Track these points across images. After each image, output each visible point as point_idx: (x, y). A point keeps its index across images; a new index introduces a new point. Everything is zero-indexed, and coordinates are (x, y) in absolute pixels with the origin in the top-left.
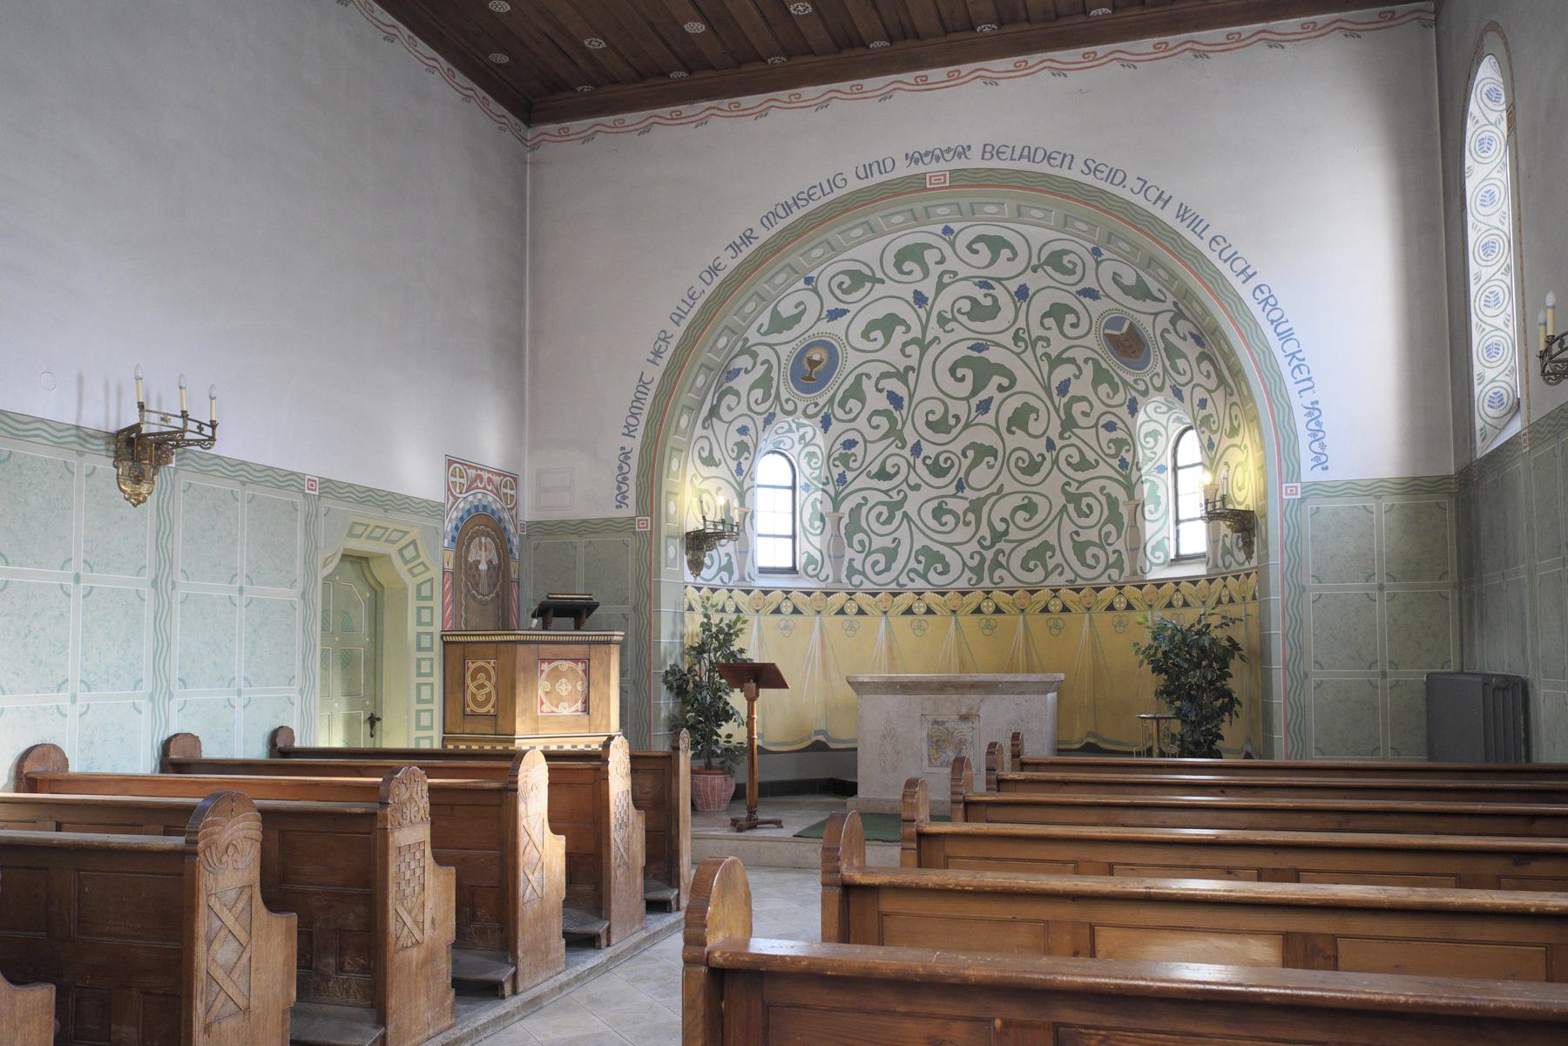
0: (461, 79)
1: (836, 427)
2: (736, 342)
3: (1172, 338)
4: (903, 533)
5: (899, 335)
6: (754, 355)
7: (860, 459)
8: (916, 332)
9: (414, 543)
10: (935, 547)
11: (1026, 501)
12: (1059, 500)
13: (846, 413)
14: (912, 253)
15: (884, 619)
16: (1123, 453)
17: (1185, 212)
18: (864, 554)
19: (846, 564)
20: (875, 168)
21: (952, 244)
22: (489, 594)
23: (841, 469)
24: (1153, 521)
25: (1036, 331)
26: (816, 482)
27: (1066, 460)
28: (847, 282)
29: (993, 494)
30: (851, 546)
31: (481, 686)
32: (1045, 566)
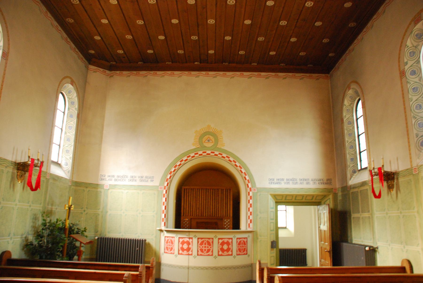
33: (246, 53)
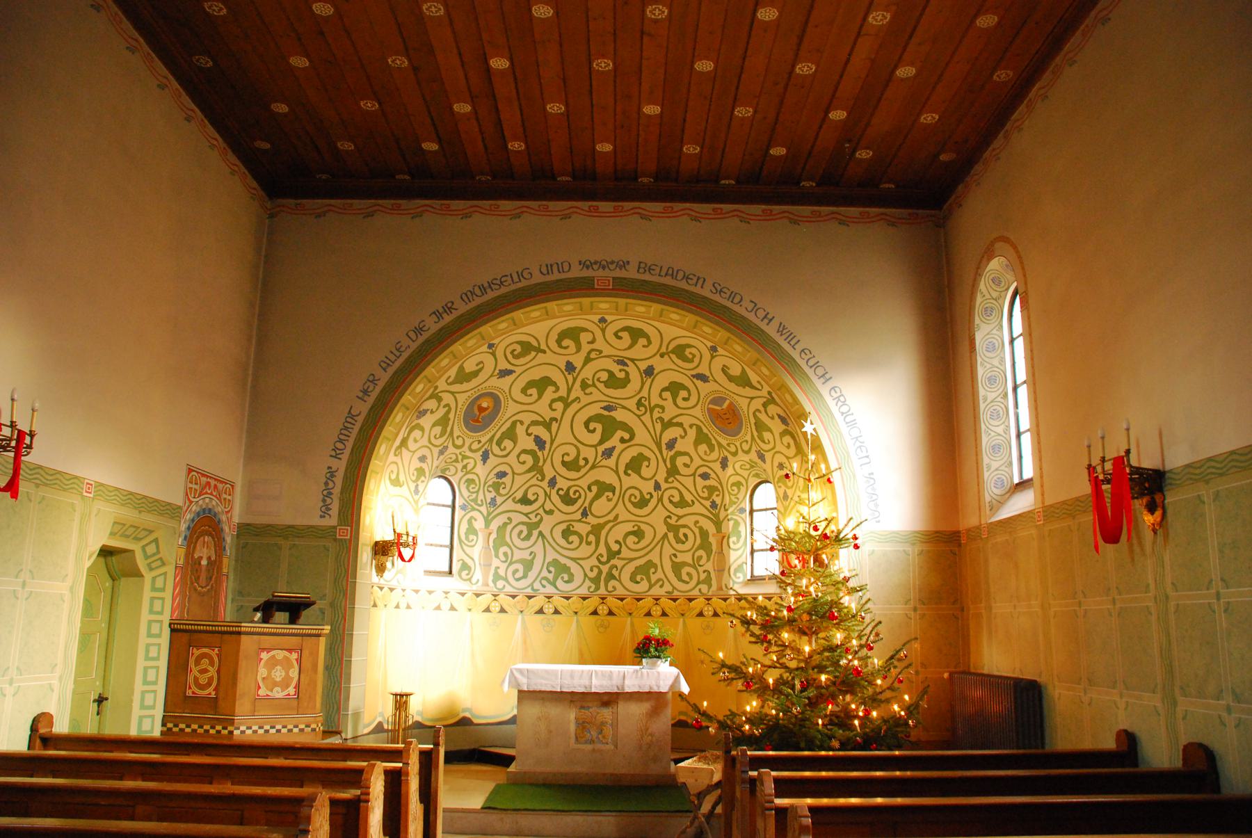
0: (232, 158)
1: (492, 460)
2: (429, 389)
3: (763, 417)
4: (538, 548)
5: (549, 393)
6: (440, 400)
7: (508, 488)
8: (563, 392)
9: (156, 541)
10: (563, 560)
11: (636, 528)
12: (662, 530)
13: (501, 450)
14: (572, 334)
15: (520, 617)
16: (714, 497)
17: (784, 329)
18: (507, 564)
19: (492, 571)
20: (555, 267)
21: (603, 331)
22: (205, 587)
23: (493, 494)
24: (734, 550)
25: (655, 400)
26: (472, 504)
27: (669, 499)
28: (519, 349)
29: (609, 521)
30: (497, 556)
31: (205, 671)
32: (649, 580)
33: (716, 68)
